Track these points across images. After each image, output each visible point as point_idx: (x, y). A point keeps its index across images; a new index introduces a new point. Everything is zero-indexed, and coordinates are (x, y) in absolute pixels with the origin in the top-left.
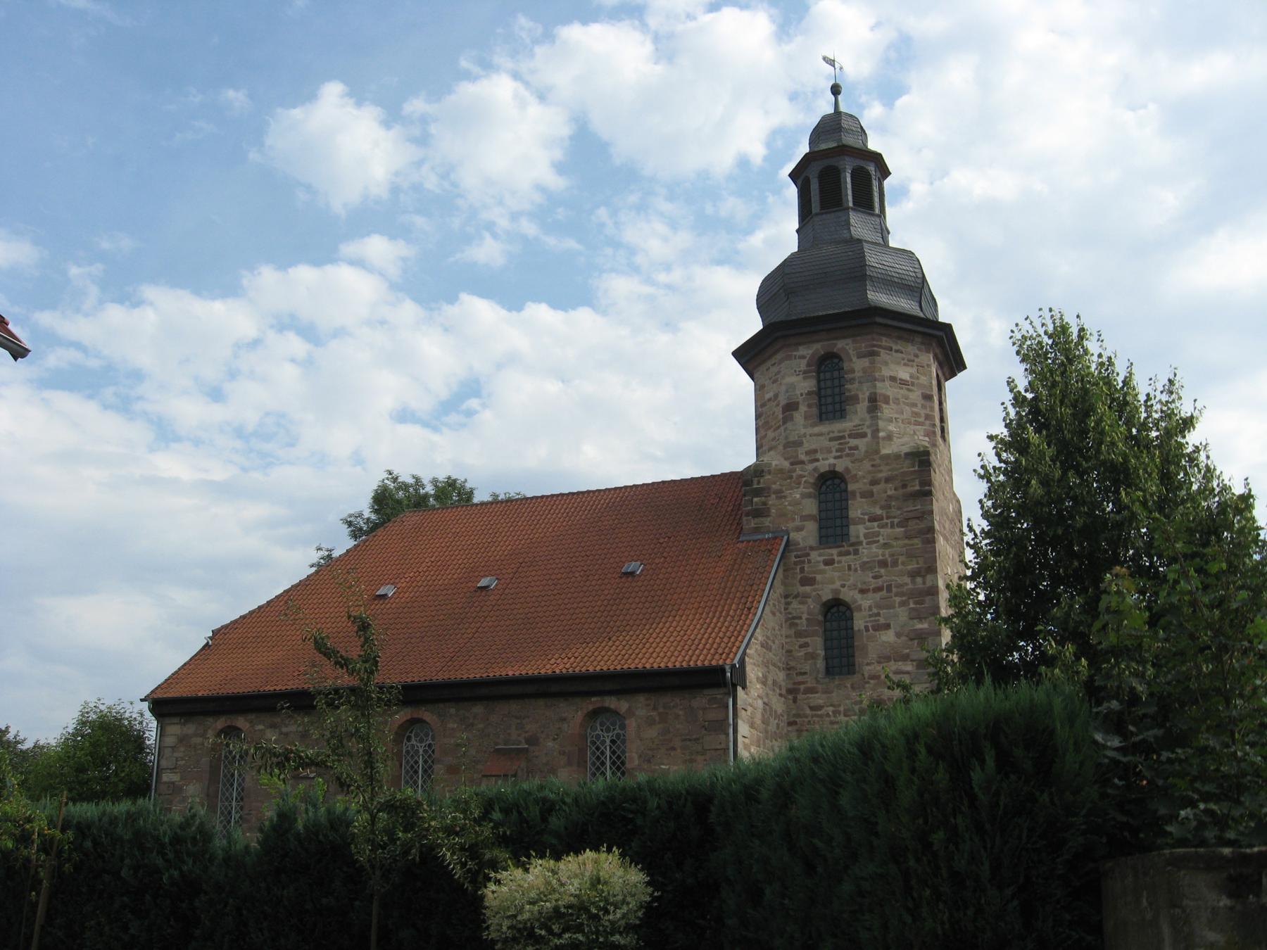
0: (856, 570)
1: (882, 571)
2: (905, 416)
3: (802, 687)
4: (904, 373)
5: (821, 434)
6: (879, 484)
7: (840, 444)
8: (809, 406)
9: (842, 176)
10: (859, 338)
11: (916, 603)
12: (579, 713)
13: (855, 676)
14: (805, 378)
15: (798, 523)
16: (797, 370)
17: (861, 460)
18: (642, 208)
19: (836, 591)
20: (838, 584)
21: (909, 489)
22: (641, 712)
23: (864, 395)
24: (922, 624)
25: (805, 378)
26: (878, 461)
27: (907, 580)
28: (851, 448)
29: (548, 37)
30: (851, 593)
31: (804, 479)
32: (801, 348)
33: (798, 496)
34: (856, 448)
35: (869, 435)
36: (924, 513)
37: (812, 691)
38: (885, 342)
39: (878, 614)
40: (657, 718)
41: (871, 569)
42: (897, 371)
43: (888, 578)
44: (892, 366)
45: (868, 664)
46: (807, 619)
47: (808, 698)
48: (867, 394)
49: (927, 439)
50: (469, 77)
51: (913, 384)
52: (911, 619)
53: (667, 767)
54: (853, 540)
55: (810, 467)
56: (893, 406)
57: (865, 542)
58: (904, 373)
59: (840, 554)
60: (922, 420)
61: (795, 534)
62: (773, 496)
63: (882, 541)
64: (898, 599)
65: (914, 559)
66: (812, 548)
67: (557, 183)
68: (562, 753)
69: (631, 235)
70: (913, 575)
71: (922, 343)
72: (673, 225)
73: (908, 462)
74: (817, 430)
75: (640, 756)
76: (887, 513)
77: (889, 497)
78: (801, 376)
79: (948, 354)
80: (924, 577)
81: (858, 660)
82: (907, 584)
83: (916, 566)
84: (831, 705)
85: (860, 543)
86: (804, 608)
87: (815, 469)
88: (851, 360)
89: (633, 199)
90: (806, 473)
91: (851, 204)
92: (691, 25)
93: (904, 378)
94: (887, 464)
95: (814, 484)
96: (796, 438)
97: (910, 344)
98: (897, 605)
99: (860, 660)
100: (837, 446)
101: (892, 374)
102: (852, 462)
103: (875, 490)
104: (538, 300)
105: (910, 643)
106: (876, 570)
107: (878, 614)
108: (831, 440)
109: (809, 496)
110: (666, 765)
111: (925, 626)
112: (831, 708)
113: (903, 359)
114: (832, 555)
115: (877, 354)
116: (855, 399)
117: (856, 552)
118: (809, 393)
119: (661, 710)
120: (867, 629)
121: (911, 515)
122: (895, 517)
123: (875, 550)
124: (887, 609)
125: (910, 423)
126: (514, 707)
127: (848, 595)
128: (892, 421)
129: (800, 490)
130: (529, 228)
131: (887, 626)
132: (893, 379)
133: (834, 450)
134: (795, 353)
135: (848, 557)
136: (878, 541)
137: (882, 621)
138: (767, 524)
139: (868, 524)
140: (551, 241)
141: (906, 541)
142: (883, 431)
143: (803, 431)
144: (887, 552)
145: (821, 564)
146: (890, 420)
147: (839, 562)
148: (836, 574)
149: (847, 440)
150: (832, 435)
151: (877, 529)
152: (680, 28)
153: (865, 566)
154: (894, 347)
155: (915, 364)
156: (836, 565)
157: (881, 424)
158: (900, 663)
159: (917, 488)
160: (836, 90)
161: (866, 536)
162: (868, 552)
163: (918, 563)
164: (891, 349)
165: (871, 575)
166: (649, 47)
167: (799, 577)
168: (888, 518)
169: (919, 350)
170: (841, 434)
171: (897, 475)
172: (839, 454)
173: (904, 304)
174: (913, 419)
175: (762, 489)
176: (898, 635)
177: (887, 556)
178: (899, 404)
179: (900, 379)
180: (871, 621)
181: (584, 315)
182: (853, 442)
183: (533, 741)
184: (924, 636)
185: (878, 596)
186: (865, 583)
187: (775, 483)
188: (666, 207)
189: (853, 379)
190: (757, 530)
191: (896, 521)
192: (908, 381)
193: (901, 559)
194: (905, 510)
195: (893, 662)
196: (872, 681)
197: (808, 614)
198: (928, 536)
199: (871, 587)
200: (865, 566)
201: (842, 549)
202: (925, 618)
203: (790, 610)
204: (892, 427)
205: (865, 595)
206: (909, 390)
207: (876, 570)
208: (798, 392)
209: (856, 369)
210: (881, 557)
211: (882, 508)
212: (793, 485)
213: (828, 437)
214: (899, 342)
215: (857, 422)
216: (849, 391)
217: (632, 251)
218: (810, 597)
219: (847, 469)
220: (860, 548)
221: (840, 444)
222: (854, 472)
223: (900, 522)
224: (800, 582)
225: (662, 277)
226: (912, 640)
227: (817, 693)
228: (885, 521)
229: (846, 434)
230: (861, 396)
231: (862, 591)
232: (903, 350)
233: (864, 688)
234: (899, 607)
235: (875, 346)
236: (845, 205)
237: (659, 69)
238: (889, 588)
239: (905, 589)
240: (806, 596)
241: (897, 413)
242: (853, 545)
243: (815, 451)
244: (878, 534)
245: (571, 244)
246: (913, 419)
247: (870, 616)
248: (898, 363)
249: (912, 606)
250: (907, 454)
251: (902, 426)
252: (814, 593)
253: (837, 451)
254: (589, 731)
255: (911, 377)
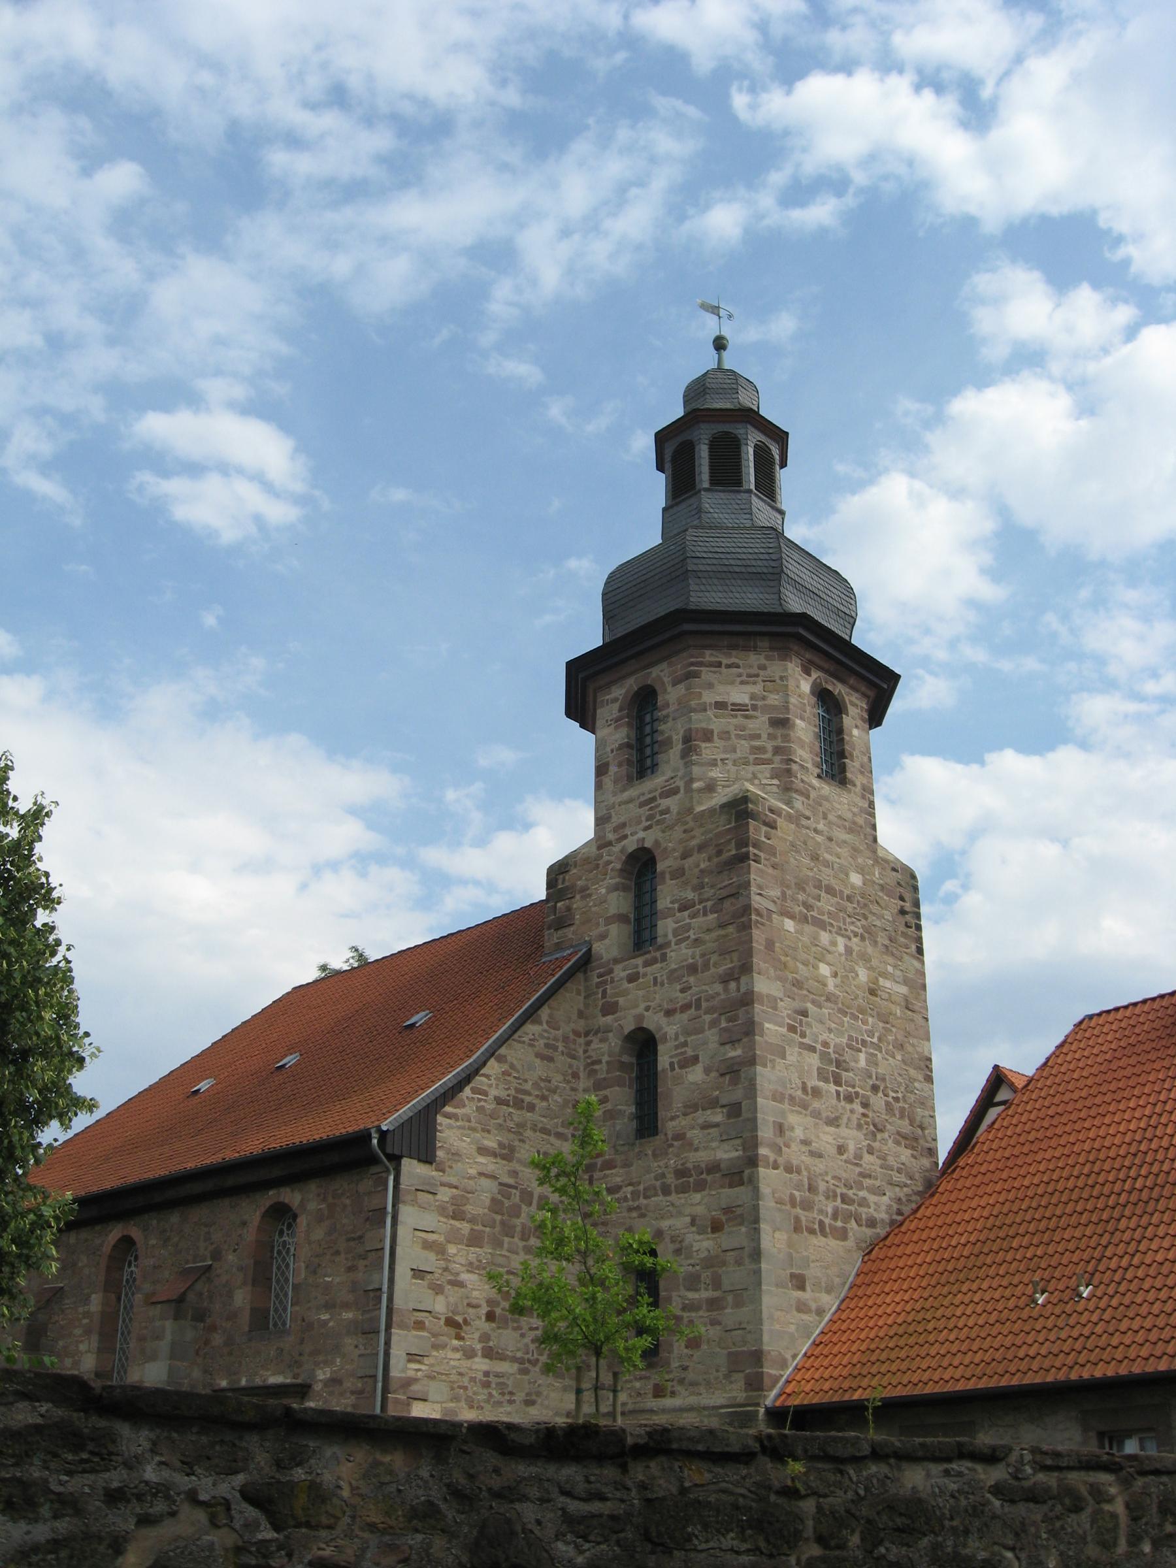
0: (662, 984)
1: (692, 979)
2: (739, 754)
3: (599, 1161)
4: (739, 695)
5: (630, 801)
6: (691, 856)
7: (651, 809)
8: (620, 765)
9: (697, 449)
10: (673, 659)
11: (729, 1020)
12: (258, 1213)
13: (658, 1137)
14: (616, 728)
15: (602, 929)
16: (609, 718)
17: (671, 828)
18: (1099, 603)
19: (640, 1018)
20: (640, 1009)
21: (726, 856)
22: (312, 1206)
23: (677, 738)
24: (735, 1049)
25: (616, 728)
26: (691, 824)
27: (718, 988)
28: (662, 813)
29: (938, 419)
30: (656, 1018)
31: (610, 867)
32: (613, 688)
33: (603, 891)
34: (667, 811)
35: (682, 791)
36: (739, 886)
37: (609, 1165)
38: (709, 656)
39: (685, 1044)
40: (326, 1212)
41: (678, 979)
42: (728, 694)
43: (697, 989)
44: (721, 688)
45: (673, 1118)
46: (608, 1062)
47: (605, 1176)
48: (682, 732)
49: (775, 782)
50: (857, 486)
51: (755, 707)
52: (723, 1044)
53: (330, 1279)
54: (660, 940)
55: (617, 849)
56: (718, 742)
57: (674, 941)
58: (739, 695)
59: (647, 964)
60: (768, 756)
61: (599, 943)
62: (578, 897)
63: (693, 937)
64: (708, 1018)
65: (727, 956)
66: (616, 961)
67: (989, 592)
68: (240, 1269)
69: (1094, 641)
70: (725, 980)
71: (772, 649)
72: (1146, 616)
73: (724, 818)
74: (626, 795)
75: (307, 1267)
76: (700, 894)
77: (702, 871)
78: (613, 726)
79: (839, 659)
80: (737, 980)
81: (662, 1114)
82: (718, 994)
83: (730, 966)
84: (630, 1184)
85: (668, 944)
86: (604, 1047)
87: (622, 851)
88: (666, 690)
89: (1085, 594)
90: (612, 858)
91: (706, 485)
92: (1108, 361)
93: (738, 701)
94: (701, 826)
95: (621, 870)
96: (605, 812)
97: (751, 654)
98: (706, 1028)
99: (664, 1113)
100: (647, 813)
101: (719, 699)
102: (663, 832)
103: (686, 866)
104: (1000, 747)
105: (721, 1080)
106: (685, 979)
107: (685, 1044)
108: (641, 805)
109: (616, 888)
110: (329, 1276)
111: (739, 1052)
112: (630, 1188)
113: (740, 675)
114: (637, 966)
115: (696, 675)
116: (668, 743)
117: (664, 958)
118: (621, 747)
119: (330, 1200)
120: (672, 1065)
121: (724, 893)
122: (708, 900)
123: (684, 951)
124: (695, 1034)
125: (746, 763)
126: (200, 1213)
127: (654, 1021)
128: (716, 765)
129: (605, 882)
130: (977, 655)
131: (695, 1060)
132: (720, 705)
133: (643, 819)
134: (607, 697)
135: (654, 966)
136: (689, 937)
137: (690, 1052)
138: (570, 936)
139: (678, 914)
140: (1005, 665)
141: (722, 932)
142: (700, 780)
143: (612, 800)
144: (698, 951)
145: (625, 982)
146: (713, 763)
147: (645, 975)
148: (641, 993)
149: (659, 801)
150: (642, 799)
151: (688, 921)
152: (1092, 368)
153: (673, 976)
154: (725, 661)
155: (760, 679)
156: (641, 980)
157: (696, 770)
158: (709, 1112)
159: (734, 852)
160: (720, 344)
161: (676, 933)
162: (679, 954)
163: (732, 962)
164: (719, 665)
165: (678, 987)
166: (1064, 401)
167: (600, 1003)
168: (700, 903)
169: (767, 658)
170: (650, 796)
171: (711, 839)
172: (649, 823)
173: (750, 599)
174: (752, 757)
175: (567, 888)
176: (707, 1071)
177: (697, 957)
178: (729, 739)
179: (733, 704)
180: (677, 1055)
181: (1066, 757)
182: (665, 803)
183: (217, 1255)
184: (736, 1068)
185: (685, 1016)
186: (671, 1001)
187: (580, 879)
188: (1132, 596)
189: (667, 716)
190: (559, 947)
191: (709, 904)
192: (747, 705)
193: (714, 958)
194: (719, 886)
195: (700, 1112)
196: (676, 1143)
197: (609, 1056)
198: (742, 920)
199: (678, 1006)
200: (673, 976)
201: (647, 956)
202: (739, 1040)
203: (590, 1053)
204: (715, 773)
205: (672, 1018)
206: (746, 717)
207: (685, 979)
208: (608, 749)
209: (671, 702)
210: (691, 961)
211: (694, 889)
212: (599, 876)
213: (637, 803)
214: (734, 652)
215: (669, 774)
216: (662, 733)
217: (1101, 660)
218: (611, 1031)
219: (657, 843)
220: (668, 951)
221: (651, 809)
222: (664, 845)
223: (714, 905)
224: (601, 1011)
225: (1151, 688)
226: (722, 1075)
227: (615, 1167)
228: (698, 907)
229: (657, 794)
230: (675, 737)
231: (669, 1013)
232: (741, 663)
233: (667, 1154)
234: (710, 1029)
235: (692, 664)
236: (745, 487)
237: (1084, 423)
238: (698, 1007)
239: (715, 1002)
240: (608, 1030)
241: (725, 752)
242: (661, 947)
243: (624, 825)
244: (688, 928)
245: (1031, 664)
246: (752, 757)
247: (677, 1047)
248: (732, 683)
249: (724, 1024)
250: (723, 806)
251: (734, 769)
252: (616, 1024)
253: (647, 820)
254: (277, 1237)
255: (752, 699)
